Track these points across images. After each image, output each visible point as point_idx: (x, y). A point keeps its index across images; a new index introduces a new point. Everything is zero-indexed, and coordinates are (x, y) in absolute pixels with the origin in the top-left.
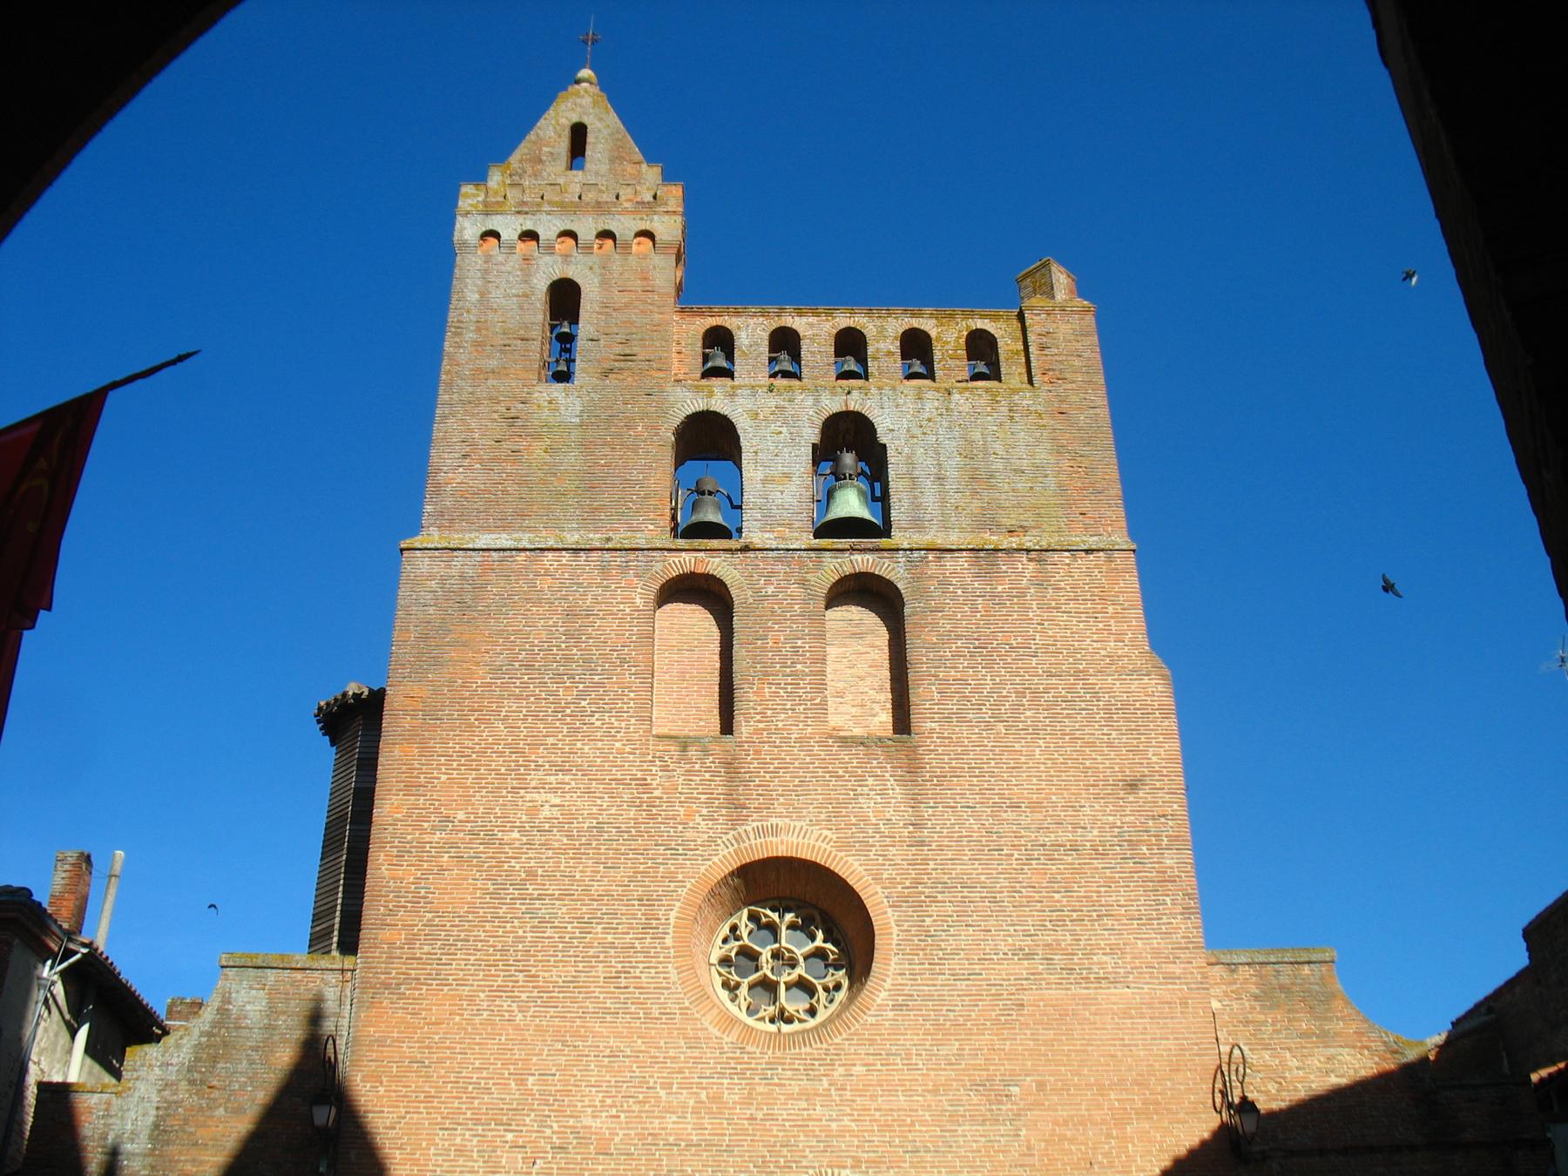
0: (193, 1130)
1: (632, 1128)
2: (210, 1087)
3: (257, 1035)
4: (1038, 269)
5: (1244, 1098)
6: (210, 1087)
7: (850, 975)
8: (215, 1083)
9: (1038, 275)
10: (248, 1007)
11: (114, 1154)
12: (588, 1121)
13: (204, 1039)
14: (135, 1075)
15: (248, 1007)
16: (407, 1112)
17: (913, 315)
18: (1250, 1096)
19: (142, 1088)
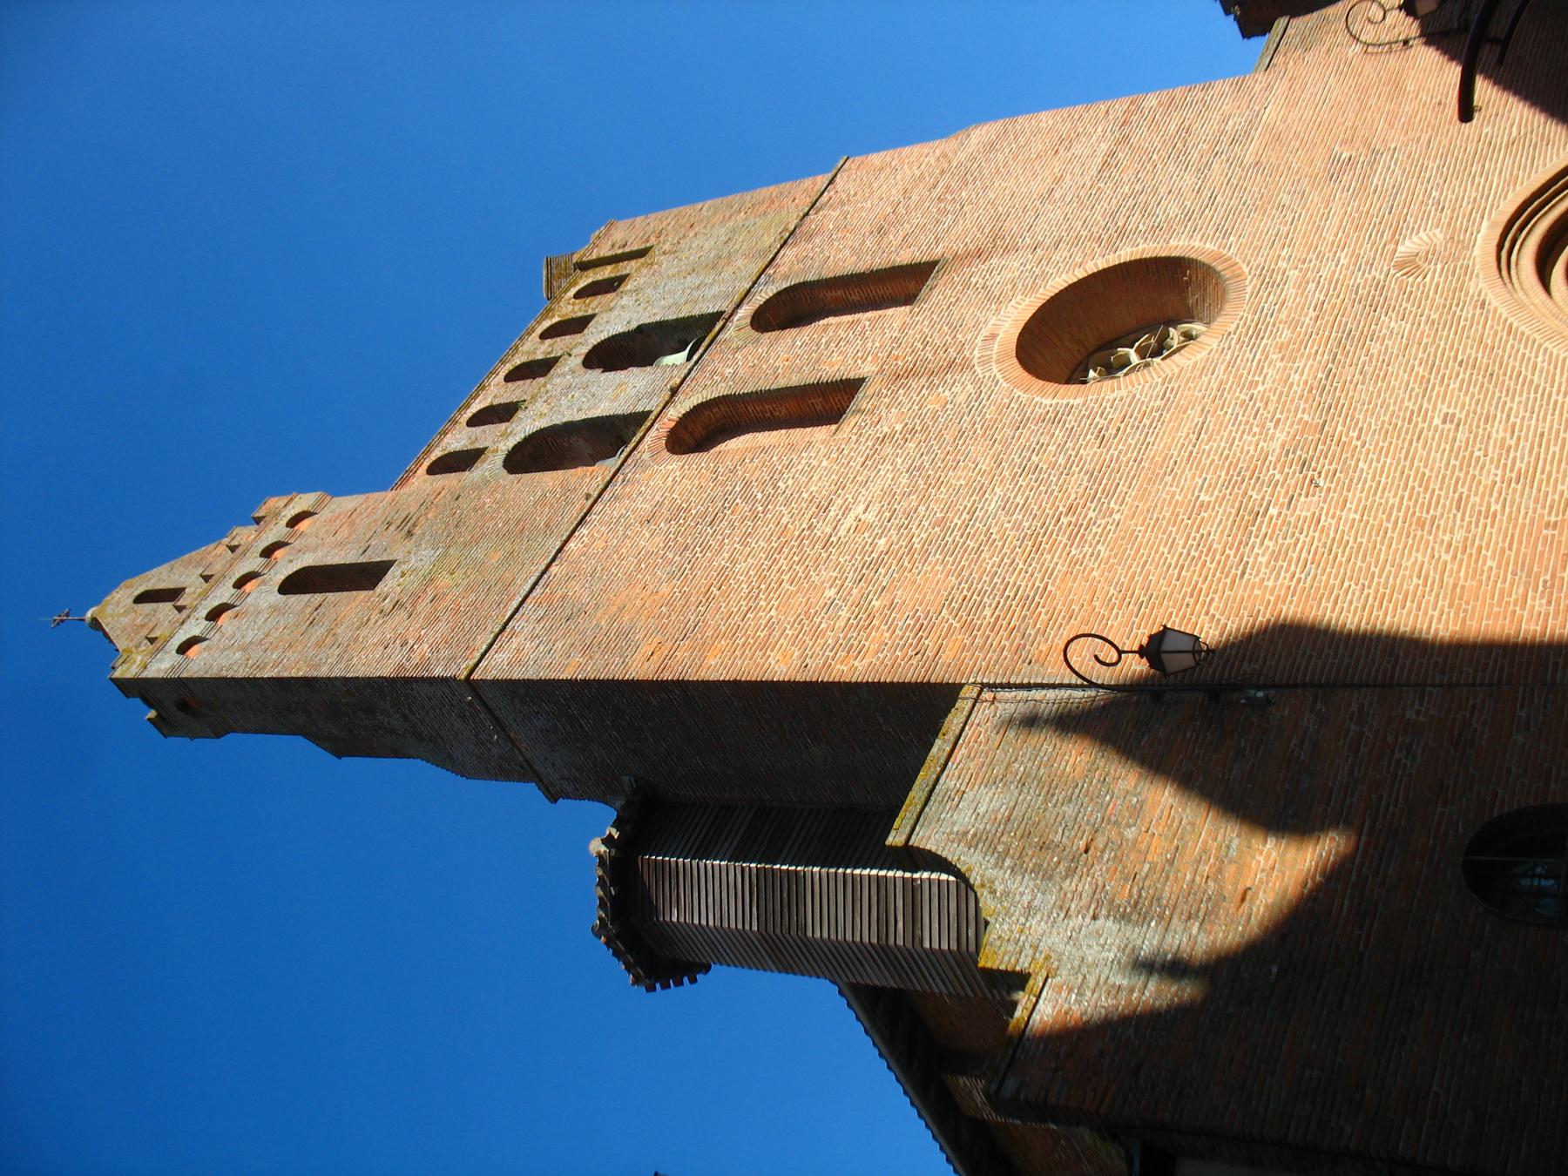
0: (1147, 866)
1: (1230, 571)
2: (1086, 851)
3: (1031, 798)
4: (549, 273)
5: (1142, 651)
6: (1086, 851)
7: (1174, 322)
8: (1082, 844)
9: (554, 271)
10: (982, 810)
11: (1147, 966)
12: (1276, 445)
13: (1008, 862)
14: (1029, 951)
15: (982, 810)
16: (1207, 613)
17: (503, 362)
18: (1135, 648)
19: (1054, 940)
